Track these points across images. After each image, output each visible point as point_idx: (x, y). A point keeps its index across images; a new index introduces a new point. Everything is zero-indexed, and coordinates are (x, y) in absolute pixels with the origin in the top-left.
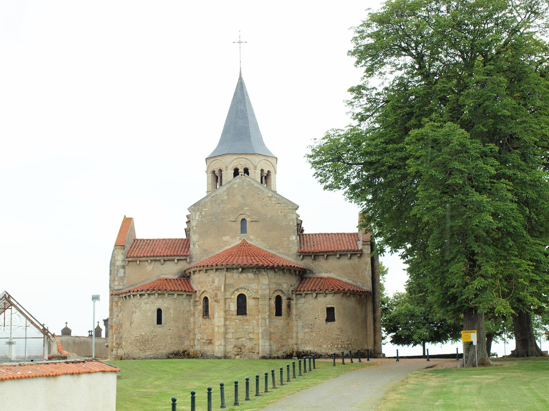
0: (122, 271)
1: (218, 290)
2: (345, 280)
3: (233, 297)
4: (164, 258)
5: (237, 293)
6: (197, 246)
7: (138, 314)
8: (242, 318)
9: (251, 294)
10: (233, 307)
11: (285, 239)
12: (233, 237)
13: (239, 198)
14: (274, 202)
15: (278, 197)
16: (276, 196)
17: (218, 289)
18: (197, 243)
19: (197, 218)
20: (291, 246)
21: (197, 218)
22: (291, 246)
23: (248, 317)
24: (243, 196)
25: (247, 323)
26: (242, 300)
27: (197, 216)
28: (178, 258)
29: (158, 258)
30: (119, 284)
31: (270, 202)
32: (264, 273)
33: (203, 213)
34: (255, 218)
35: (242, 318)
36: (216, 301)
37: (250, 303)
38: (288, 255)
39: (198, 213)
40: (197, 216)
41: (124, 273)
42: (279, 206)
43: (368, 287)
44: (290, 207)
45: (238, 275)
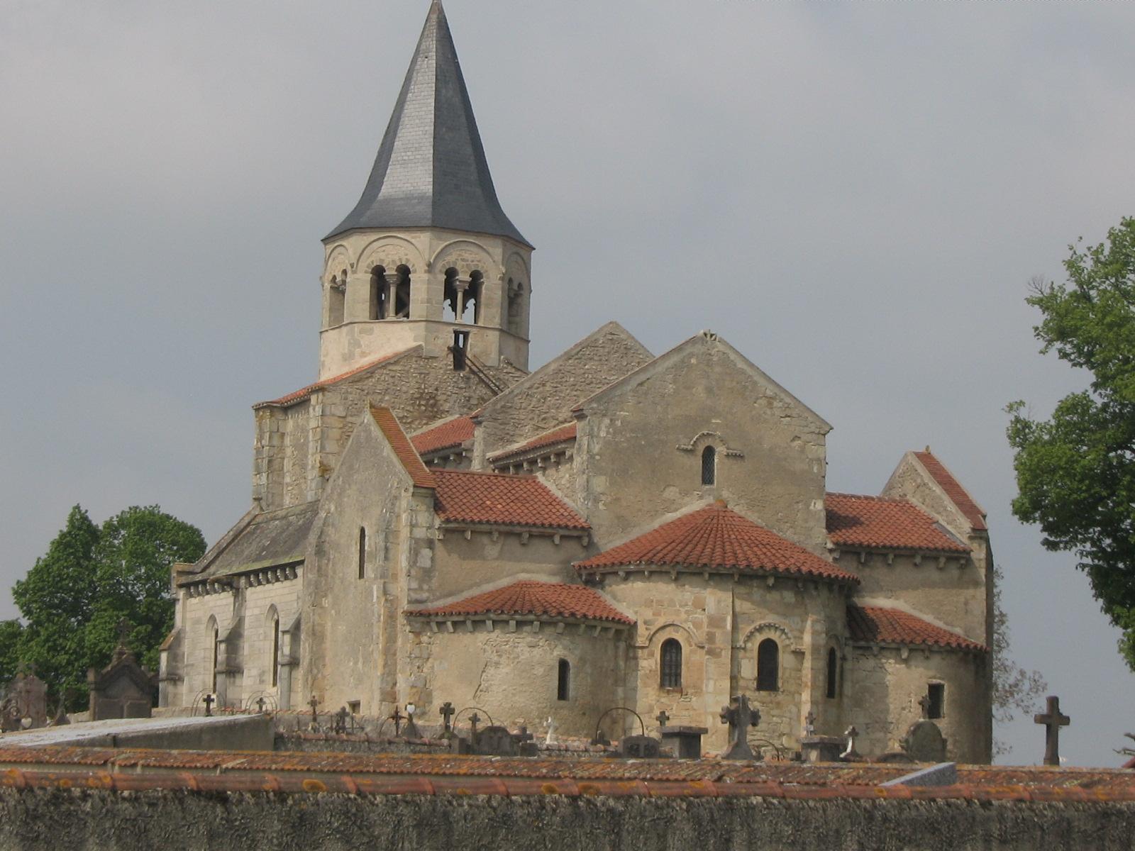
0: (426, 552)
1: (718, 627)
2: (928, 618)
3: (749, 645)
4: (534, 530)
5: (759, 638)
6: (601, 506)
7: (504, 670)
8: (768, 699)
9: (787, 642)
10: (749, 669)
11: (800, 506)
12: (685, 493)
13: (700, 391)
14: (777, 412)
15: (788, 400)
16: (783, 396)
17: (715, 622)
18: (603, 498)
19: (603, 434)
20: (811, 524)
21: (603, 434)
22: (811, 524)
23: (780, 697)
24: (709, 390)
25: (775, 712)
26: (768, 651)
27: (603, 428)
28: (562, 532)
29: (518, 529)
30: (421, 588)
31: (769, 412)
32: (814, 593)
33: (618, 423)
34: (736, 447)
35: (768, 699)
36: (710, 652)
37: (785, 660)
38: (813, 542)
39: (607, 421)
40: (603, 428)
41: (432, 559)
42: (789, 424)
43: (979, 639)
44: (812, 429)
45: (761, 592)
